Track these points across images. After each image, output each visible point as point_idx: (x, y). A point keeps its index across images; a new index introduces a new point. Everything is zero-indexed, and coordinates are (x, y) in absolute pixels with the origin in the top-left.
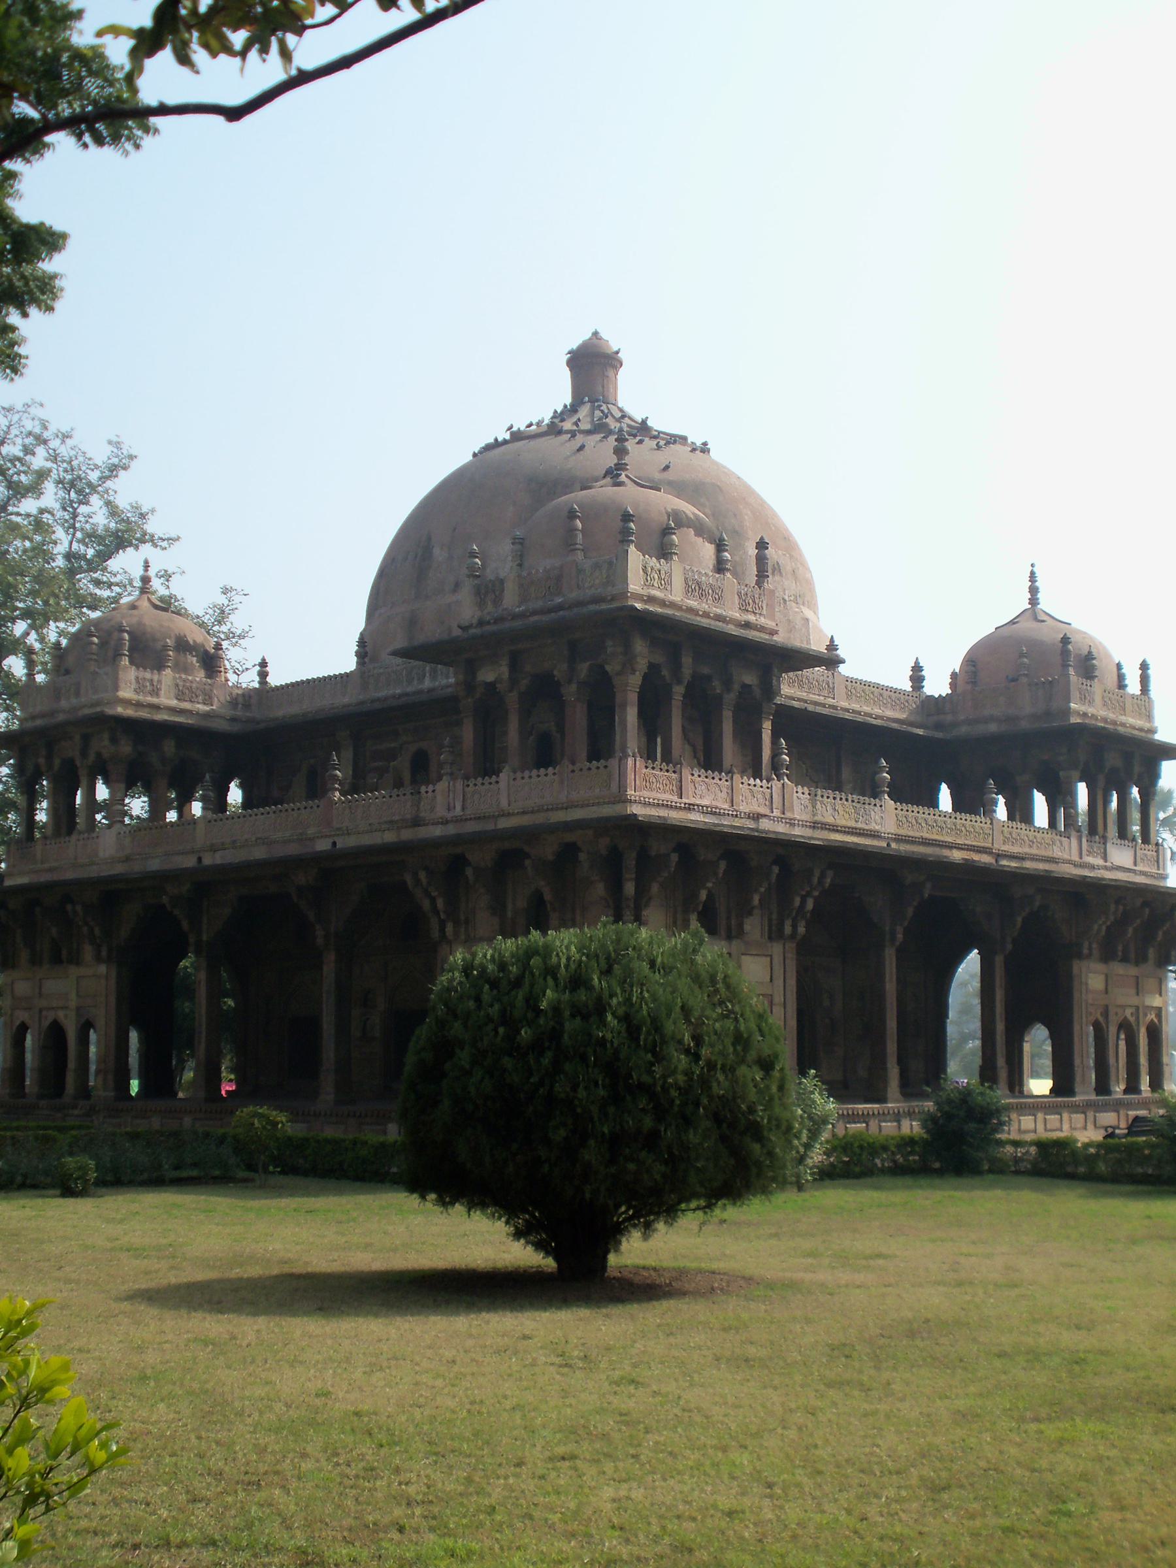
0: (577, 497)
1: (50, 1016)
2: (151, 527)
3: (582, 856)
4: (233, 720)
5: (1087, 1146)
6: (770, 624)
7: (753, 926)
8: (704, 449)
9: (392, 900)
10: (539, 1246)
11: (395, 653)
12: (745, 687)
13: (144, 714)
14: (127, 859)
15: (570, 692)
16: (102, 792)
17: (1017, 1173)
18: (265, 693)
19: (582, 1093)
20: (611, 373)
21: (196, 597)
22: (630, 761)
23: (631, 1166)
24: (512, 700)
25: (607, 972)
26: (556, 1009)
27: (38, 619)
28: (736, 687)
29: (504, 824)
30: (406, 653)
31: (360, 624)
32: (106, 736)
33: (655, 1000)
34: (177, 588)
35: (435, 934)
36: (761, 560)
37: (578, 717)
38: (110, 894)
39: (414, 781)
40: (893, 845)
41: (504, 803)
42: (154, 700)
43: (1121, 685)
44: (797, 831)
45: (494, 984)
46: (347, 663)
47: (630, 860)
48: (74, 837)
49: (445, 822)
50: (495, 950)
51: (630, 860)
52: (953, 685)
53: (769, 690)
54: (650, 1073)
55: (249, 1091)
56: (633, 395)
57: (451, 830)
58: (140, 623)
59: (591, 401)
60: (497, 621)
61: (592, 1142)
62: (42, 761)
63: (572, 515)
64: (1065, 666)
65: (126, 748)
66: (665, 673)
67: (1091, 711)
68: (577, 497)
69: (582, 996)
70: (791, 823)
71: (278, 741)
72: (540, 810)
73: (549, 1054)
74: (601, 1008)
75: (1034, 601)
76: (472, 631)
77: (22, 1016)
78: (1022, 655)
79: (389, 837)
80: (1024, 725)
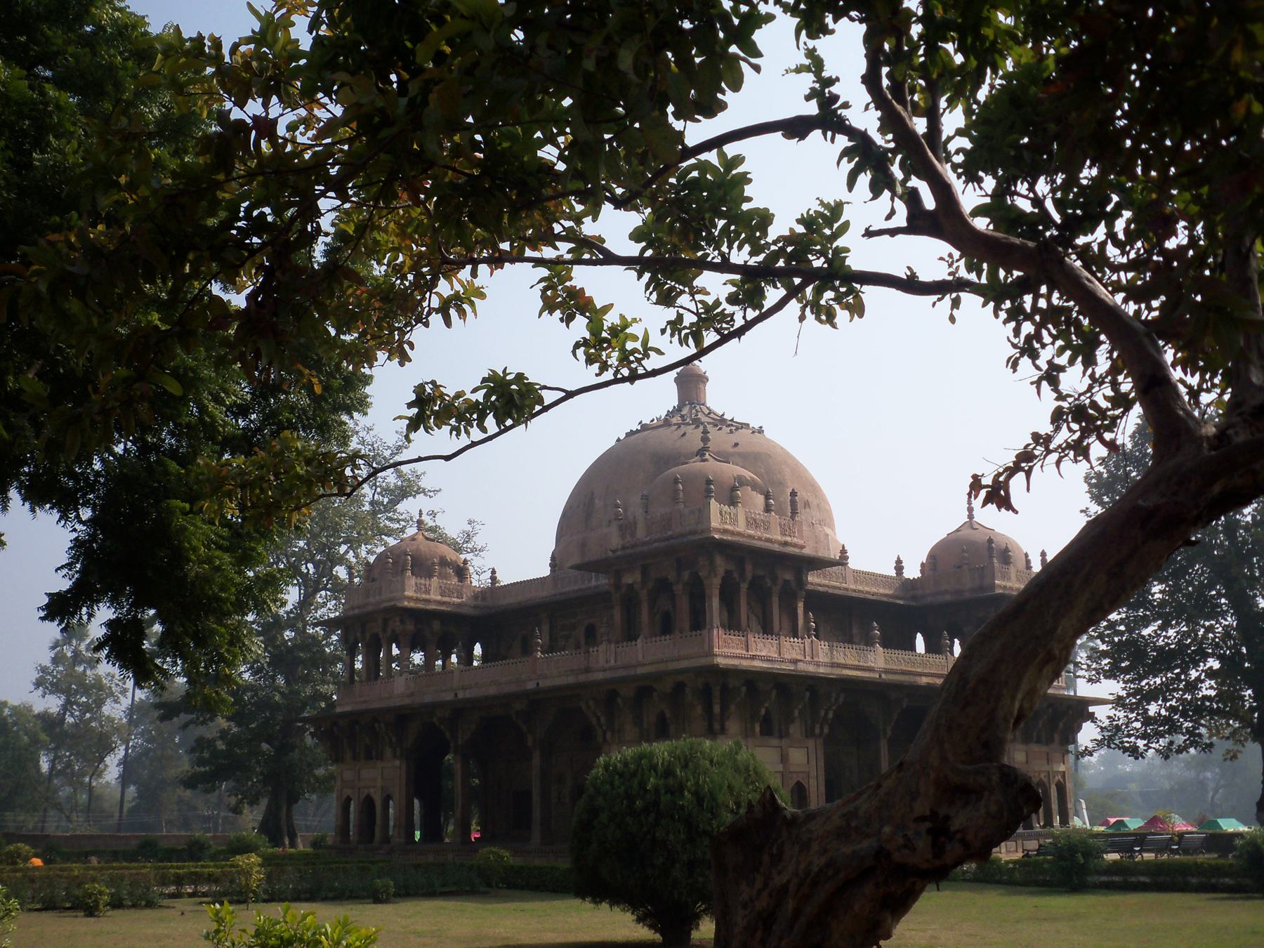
0: (677, 470)
2: (423, 483)
3: (687, 690)
4: (475, 607)
5: (1007, 862)
6: (801, 542)
7: (795, 729)
8: (760, 431)
9: (572, 719)
10: (651, 927)
11: (571, 568)
12: (786, 581)
13: (420, 606)
14: (412, 694)
15: (678, 589)
16: (395, 651)
17: (964, 880)
18: (494, 589)
19: (671, 837)
20: (701, 386)
21: (452, 528)
22: (715, 632)
23: (700, 879)
24: (644, 595)
25: (685, 766)
26: (656, 790)
27: (353, 544)
28: (780, 582)
29: (640, 671)
30: (578, 567)
31: (551, 545)
32: (397, 619)
33: (712, 781)
34: (440, 521)
35: (600, 739)
36: (793, 504)
37: (684, 604)
38: (401, 717)
39: (587, 643)
40: (883, 676)
41: (640, 658)
42: (427, 597)
43: (1029, 567)
44: (822, 670)
45: (621, 775)
46: (546, 572)
47: (717, 692)
48: (379, 682)
49: (604, 670)
50: (620, 754)
51: (717, 692)
52: (922, 571)
53: (801, 582)
54: (711, 825)
55: (489, 837)
57: (608, 675)
58: (418, 550)
59: (691, 404)
60: (633, 546)
61: (678, 865)
62: (359, 635)
63: (676, 481)
64: (991, 557)
65: (410, 627)
66: (736, 575)
67: (1009, 584)
68: (677, 470)
69: (671, 781)
70: (818, 664)
71: (504, 620)
72: (662, 661)
73: (653, 815)
74: (681, 788)
75: (971, 516)
76: (619, 553)
77: (348, 792)
78: (963, 551)
79: (571, 680)
80: (967, 595)
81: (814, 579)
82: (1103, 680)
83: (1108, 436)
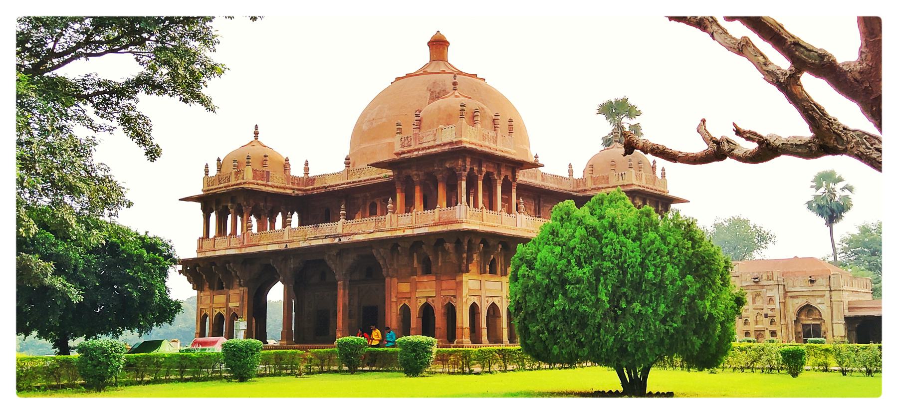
1: (491, 301)
7: (473, 268)
35: (384, 273)
46: (339, 166)
56: (455, 57)
81: (523, 177)
82: (135, 140)
83: (832, 185)
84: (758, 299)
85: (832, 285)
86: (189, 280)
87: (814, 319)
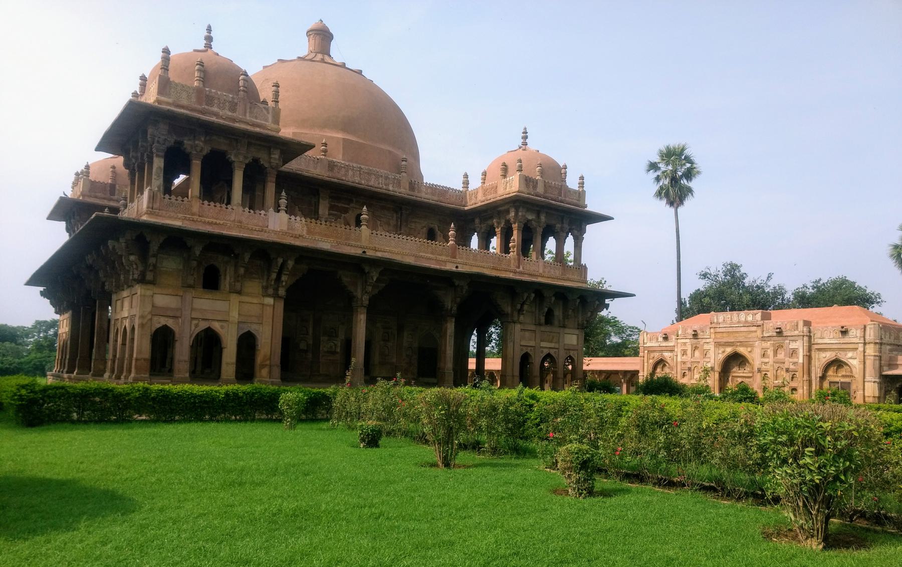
56: (339, 52)
84: (779, 351)
85: (867, 337)
86: (52, 303)
87: (843, 376)
